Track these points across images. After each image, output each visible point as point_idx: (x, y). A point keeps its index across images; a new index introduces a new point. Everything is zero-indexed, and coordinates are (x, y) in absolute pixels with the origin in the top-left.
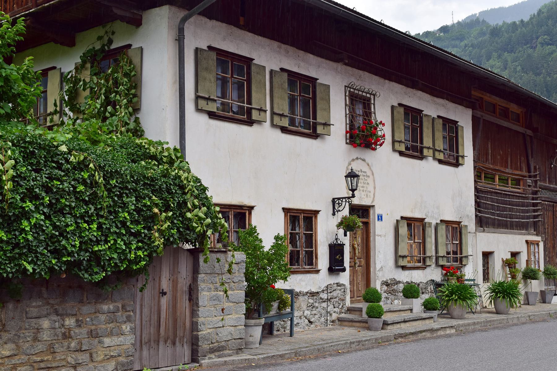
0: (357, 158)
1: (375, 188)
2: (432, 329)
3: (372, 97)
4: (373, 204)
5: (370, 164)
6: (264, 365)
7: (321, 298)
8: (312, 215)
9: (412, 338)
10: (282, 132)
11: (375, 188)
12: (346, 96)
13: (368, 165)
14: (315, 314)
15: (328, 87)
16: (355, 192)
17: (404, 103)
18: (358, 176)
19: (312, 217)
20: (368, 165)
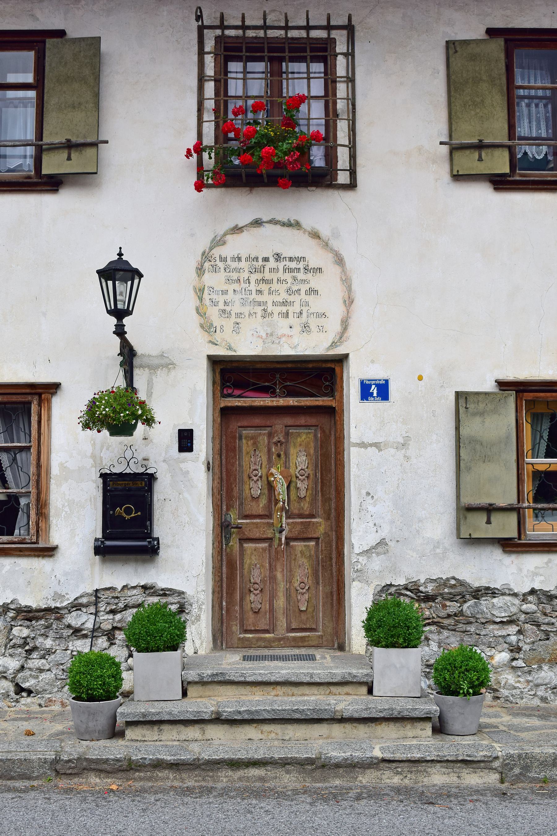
0: (257, 223)
1: (349, 302)
2: (310, 761)
3: (340, 37)
4: (340, 350)
5: (325, 232)
6: (398, 790)
7: (69, 626)
8: (29, 398)
9: (170, 779)
10: (496, 189)
11: (349, 302)
12: (201, 53)
13: (315, 235)
14: (41, 671)
15: (94, 43)
16: (126, 321)
17: (499, 24)
18: (136, 274)
19: (30, 403)
20: (315, 235)
